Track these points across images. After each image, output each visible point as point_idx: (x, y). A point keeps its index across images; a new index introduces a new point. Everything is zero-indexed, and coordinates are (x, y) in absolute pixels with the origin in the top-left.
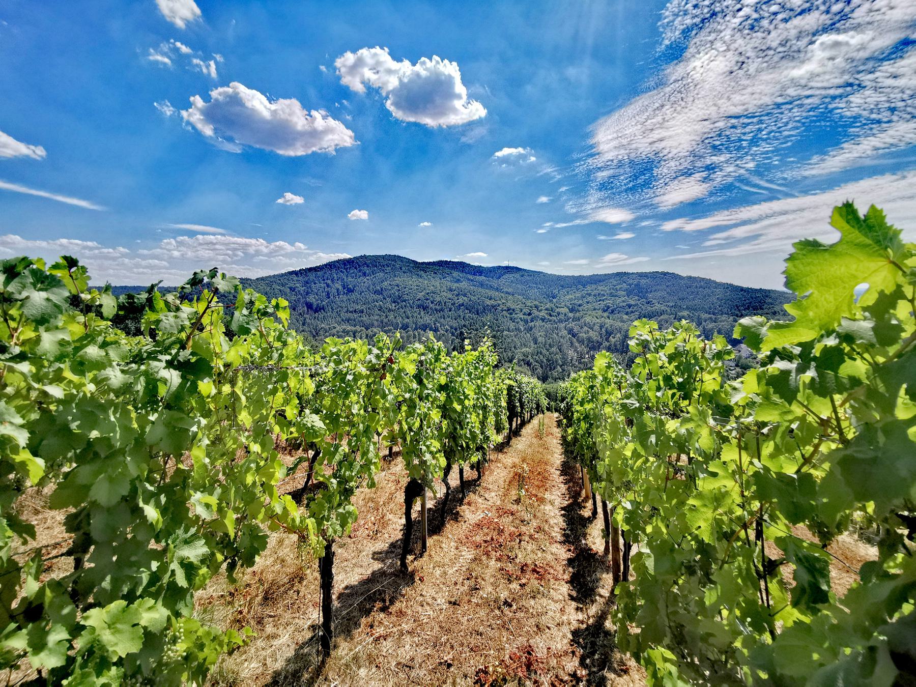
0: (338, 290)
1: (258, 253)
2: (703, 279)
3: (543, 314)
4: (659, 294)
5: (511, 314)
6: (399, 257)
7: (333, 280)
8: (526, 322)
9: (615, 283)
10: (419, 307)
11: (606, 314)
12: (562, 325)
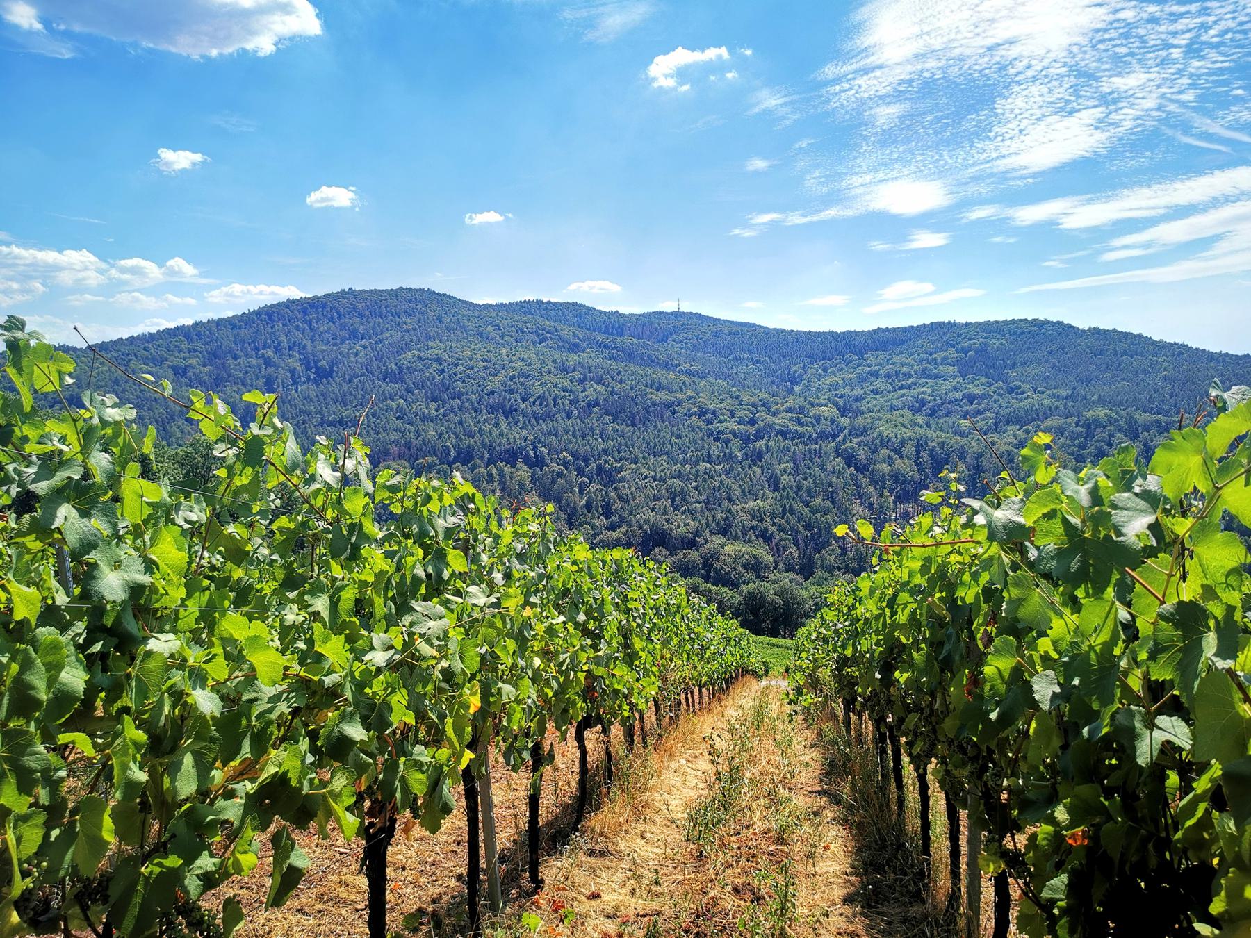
0: (293, 371)
1: (79, 288)
2: (1126, 335)
3: (781, 420)
4: (1033, 370)
5: (709, 422)
6: (430, 292)
7: (277, 349)
8: (746, 439)
9: (930, 347)
10: (493, 409)
11: (920, 419)
12: (829, 446)
